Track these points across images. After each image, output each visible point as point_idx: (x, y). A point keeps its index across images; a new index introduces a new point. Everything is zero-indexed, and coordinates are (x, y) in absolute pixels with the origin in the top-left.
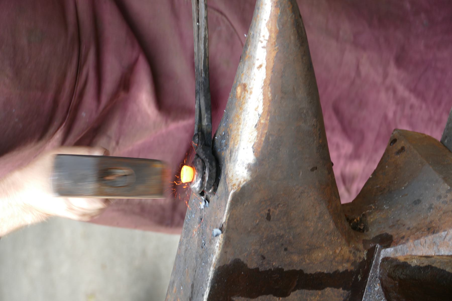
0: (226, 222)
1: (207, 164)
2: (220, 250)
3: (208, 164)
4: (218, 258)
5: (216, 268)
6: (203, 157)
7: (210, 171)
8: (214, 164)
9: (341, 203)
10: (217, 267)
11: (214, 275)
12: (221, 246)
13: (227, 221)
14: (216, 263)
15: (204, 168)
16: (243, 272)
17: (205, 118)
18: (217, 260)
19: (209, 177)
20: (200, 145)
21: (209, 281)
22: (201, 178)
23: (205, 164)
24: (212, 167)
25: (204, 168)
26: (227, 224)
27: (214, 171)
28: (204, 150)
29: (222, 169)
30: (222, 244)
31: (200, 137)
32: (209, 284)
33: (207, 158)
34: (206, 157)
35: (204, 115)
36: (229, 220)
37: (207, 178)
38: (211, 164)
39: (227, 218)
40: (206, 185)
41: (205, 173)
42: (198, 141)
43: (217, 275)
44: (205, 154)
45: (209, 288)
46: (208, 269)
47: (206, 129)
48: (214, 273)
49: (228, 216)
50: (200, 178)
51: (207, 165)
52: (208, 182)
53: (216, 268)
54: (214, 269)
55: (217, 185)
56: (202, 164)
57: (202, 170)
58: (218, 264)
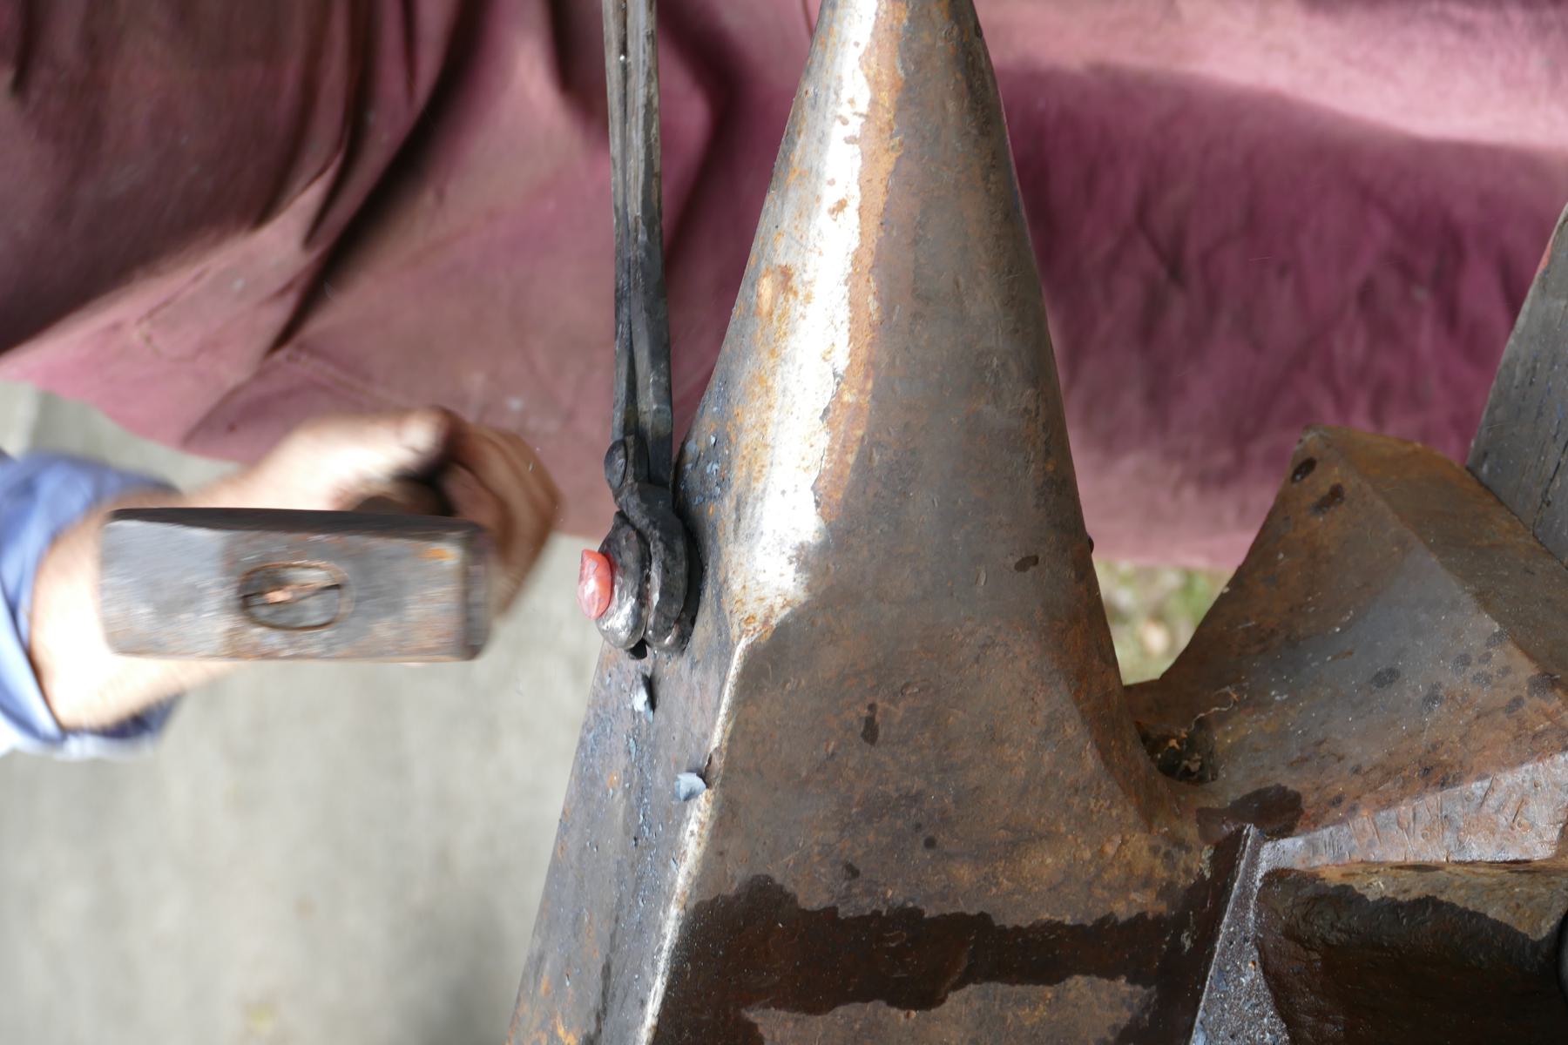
0: (723, 747)
1: (655, 546)
2: (703, 845)
3: (660, 546)
4: (695, 872)
8: (680, 546)
10: (692, 904)
11: (680, 931)
12: (705, 833)
13: (725, 744)
14: (688, 892)
15: (645, 561)
18: (690, 881)
20: (630, 480)
24: (674, 558)
25: (645, 561)
26: (725, 753)
28: (643, 498)
29: (707, 564)
30: (709, 825)
31: (631, 452)
33: (655, 528)
36: (731, 739)
37: (655, 597)
38: (669, 548)
39: (727, 736)
41: (648, 578)
42: (623, 467)
44: (649, 512)
45: (665, 979)
46: (661, 913)
48: (680, 927)
49: (730, 726)
51: (657, 549)
54: (682, 913)
56: (640, 548)
58: (695, 894)
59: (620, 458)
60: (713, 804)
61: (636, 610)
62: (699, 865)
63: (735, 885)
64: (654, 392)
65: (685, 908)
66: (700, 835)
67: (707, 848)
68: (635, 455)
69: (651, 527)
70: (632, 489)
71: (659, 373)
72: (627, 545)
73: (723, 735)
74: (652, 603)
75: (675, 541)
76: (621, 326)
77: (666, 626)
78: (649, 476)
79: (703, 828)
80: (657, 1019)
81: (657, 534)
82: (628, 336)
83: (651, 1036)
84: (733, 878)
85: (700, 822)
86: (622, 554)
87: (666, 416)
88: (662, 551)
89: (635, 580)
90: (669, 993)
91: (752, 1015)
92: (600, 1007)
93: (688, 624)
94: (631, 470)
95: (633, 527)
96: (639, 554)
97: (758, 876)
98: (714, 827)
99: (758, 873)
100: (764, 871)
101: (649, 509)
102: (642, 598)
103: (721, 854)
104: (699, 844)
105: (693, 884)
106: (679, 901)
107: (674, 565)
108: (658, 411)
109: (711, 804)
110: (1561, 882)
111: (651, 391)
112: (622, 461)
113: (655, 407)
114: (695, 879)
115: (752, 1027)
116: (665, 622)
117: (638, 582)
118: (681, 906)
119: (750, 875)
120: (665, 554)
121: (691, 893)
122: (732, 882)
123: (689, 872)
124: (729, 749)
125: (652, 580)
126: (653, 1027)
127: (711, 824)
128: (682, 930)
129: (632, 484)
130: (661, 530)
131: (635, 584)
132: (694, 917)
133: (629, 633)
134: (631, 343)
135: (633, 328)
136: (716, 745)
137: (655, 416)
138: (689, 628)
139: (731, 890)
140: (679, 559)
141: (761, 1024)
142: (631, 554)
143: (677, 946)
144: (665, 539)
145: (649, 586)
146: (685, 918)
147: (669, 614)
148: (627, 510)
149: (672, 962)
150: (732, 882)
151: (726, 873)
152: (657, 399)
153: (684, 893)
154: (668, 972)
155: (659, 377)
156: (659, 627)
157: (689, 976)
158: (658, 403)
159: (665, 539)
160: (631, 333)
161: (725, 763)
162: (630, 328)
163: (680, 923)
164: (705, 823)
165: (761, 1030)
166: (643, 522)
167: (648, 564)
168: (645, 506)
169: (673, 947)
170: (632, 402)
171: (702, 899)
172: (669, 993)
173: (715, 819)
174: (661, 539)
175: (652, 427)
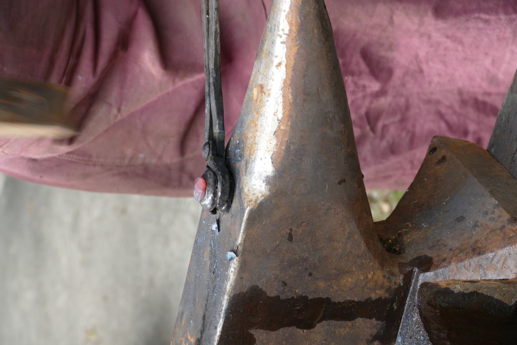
0: (242, 243)
1: (219, 177)
2: (235, 275)
3: (221, 177)
4: (233, 284)
5: (230, 297)
6: (215, 169)
8: (227, 177)
10: (232, 295)
11: (228, 304)
12: (236, 271)
13: (243, 242)
14: (231, 291)
15: (216, 182)
18: (231, 287)
20: (211, 155)
23: (217, 177)
25: (216, 182)
26: (242, 245)
30: (238, 269)
31: (211, 146)
33: (219, 171)
35: (216, 121)
36: (245, 240)
38: (224, 177)
39: (243, 239)
40: (218, 201)
41: (217, 188)
42: (208, 151)
44: (217, 166)
47: (218, 136)
48: (228, 303)
49: (244, 236)
51: (220, 178)
52: (220, 198)
54: (229, 298)
56: (214, 178)
57: (214, 184)
58: (233, 292)
59: (207, 148)
60: (239, 262)
64: (218, 126)
66: (235, 272)
67: (237, 276)
68: (212, 147)
69: (218, 171)
72: (210, 177)
73: (242, 239)
79: (235, 270)
80: (221, 333)
83: (219, 339)
84: (246, 286)
88: (221, 179)
89: (212, 188)
92: (202, 329)
93: (230, 202)
97: (254, 286)
98: (239, 269)
99: (254, 284)
100: (256, 284)
101: (217, 165)
102: (215, 194)
103: (241, 278)
104: (234, 275)
109: (238, 262)
111: (217, 126)
114: (233, 286)
115: (252, 335)
120: (222, 179)
121: (232, 291)
122: (245, 287)
124: (244, 244)
130: (221, 172)
136: (240, 242)
137: (219, 134)
141: (255, 334)
143: (227, 309)
145: (217, 190)
146: (230, 300)
148: (210, 165)
149: (225, 314)
154: (224, 317)
155: (220, 121)
157: (231, 318)
159: (222, 174)
160: (210, 107)
161: (243, 248)
162: (210, 105)
163: (228, 301)
164: (236, 268)
165: (255, 336)
166: (215, 169)
168: (215, 164)
169: (226, 309)
172: (225, 324)
173: (239, 267)
174: (221, 175)
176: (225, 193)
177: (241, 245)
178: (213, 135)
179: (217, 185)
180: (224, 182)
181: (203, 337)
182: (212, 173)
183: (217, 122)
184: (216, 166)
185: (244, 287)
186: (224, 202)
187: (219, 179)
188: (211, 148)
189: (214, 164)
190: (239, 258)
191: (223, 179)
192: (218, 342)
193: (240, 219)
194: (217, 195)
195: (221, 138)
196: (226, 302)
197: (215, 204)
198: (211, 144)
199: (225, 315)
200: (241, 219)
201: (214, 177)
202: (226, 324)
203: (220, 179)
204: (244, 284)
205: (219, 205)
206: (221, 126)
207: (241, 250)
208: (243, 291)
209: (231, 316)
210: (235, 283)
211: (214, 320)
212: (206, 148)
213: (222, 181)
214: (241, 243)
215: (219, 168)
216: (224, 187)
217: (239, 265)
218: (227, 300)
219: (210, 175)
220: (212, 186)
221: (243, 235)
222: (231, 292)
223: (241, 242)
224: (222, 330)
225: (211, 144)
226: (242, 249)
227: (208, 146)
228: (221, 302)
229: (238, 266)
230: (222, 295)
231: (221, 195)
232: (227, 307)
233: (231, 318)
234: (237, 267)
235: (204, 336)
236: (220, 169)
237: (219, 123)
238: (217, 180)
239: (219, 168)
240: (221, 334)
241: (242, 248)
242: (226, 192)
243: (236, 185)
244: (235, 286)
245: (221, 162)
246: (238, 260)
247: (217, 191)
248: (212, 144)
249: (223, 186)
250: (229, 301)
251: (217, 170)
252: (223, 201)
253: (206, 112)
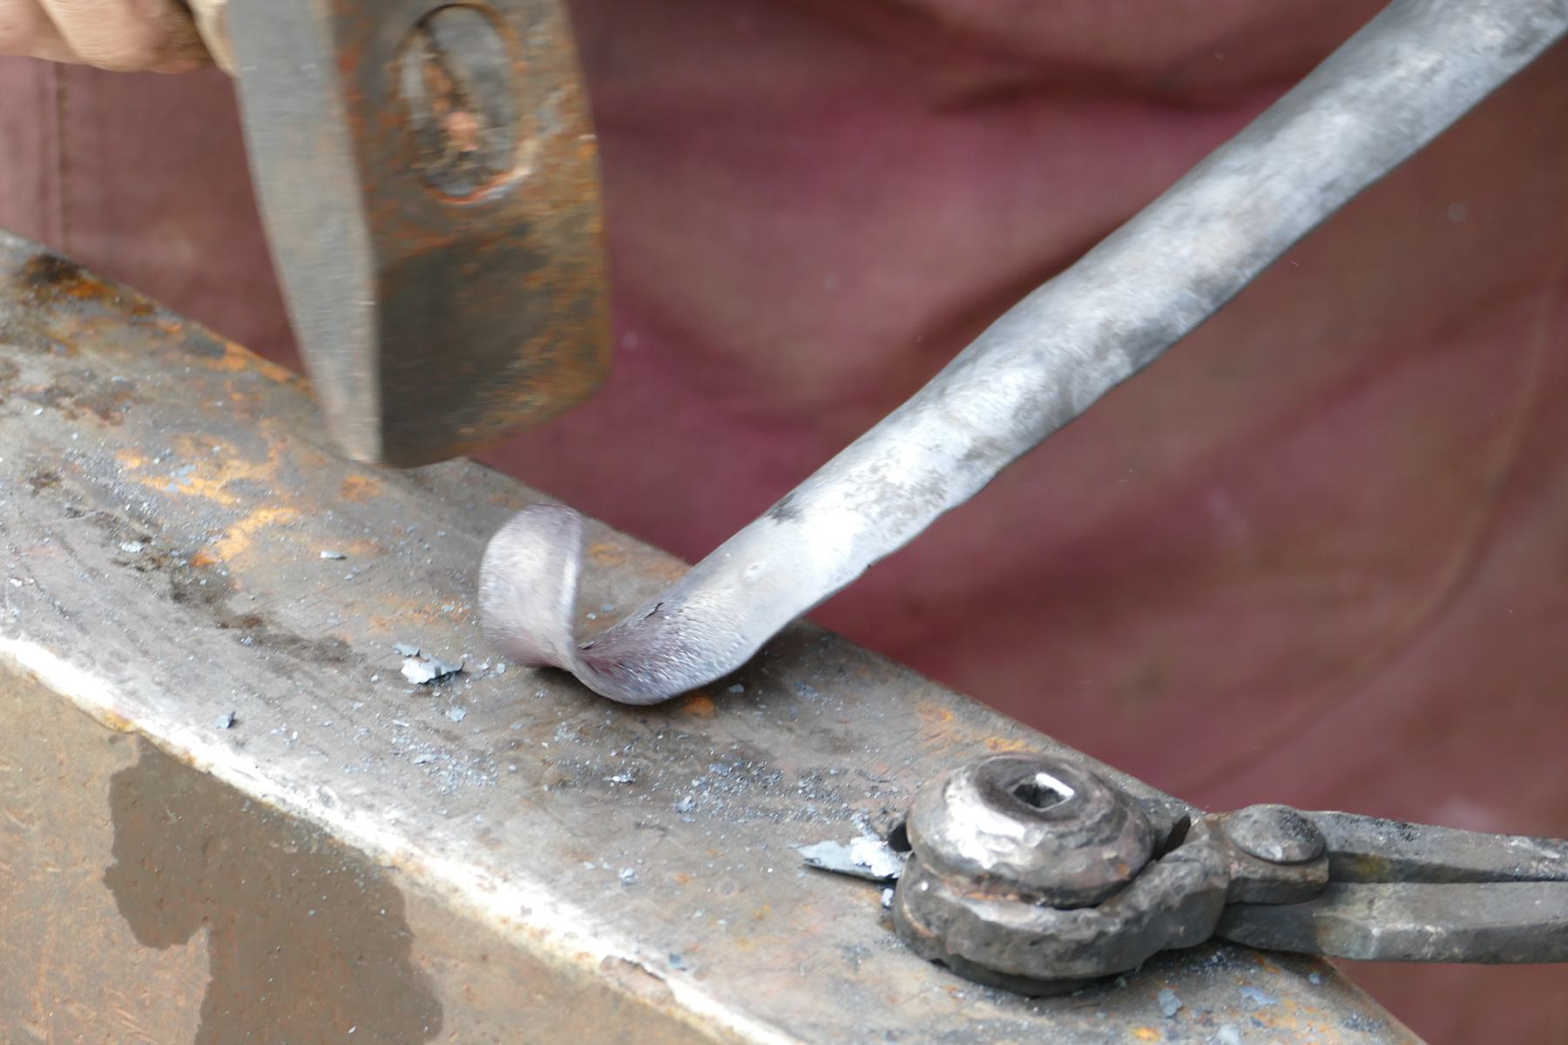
0: (673, 1008)
1: (1089, 922)
2: (502, 929)
3: (1087, 934)
4: (455, 901)
5: (390, 872)
6: (1143, 897)
7: (1037, 940)
8: (1083, 968)
9: (894, 894)
10: (399, 881)
11: (353, 849)
12: (522, 938)
13: (678, 1015)
14: (422, 881)
15: (1064, 898)
16: (315, 915)
17: (1419, 916)
18: (441, 889)
19: (993, 927)
20: (1236, 869)
21: (316, 811)
22: (994, 866)
23: (1093, 906)
24: (1059, 957)
25: (1064, 898)
26: (663, 1009)
27: (1034, 966)
28: (1191, 900)
29: (1041, 1013)
30: (537, 949)
31: (1293, 874)
32: (303, 803)
33: (1127, 922)
34: (1138, 917)
35: (1441, 915)
36: (685, 1029)
37: (988, 912)
38: (1083, 949)
39: (693, 1021)
40: (947, 894)
41: (1027, 898)
42: (1264, 855)
43: (351, 873)
44: (1162, 910)
45: (271, 800)
46: (396, 814)
47: (1345, 922)
48: (361, 852)
49: (709, 1031)
50: (995, 860)
51: (1086, 923)
52: (964, 912)
53: (390, 872)
54: (386, 861)
55: (944, 959)
56: (1091, 889)
57: (1047, 884)
58: (417, 892)
59: (1284, 850)
60: (574, 967)
61: (969, 867)
62: (467, 913)
63: (429, 970)
64: (1406, 932)
65: (393, 867)
66: (519, 927)
67: (496, 934)
68: (1286, 882)
69: (1129, 914)
70: (1216, 874)
71: (1445, 943)
72: (1102, 862)
73: (695, 1015)
74: (977, 901)
75: (1095, 960)
76: (1556, 856)
77: (933, 918)
78: (1241, 903)
79: (533, 935)
80: (203, 770)
81: (1113, 929)
82: (1532, 872)
83: (175, 752)
84: (441, 968)
85: (543, 933)
86: (1086, 849)
87: (1354, 951)
88: (1076, 936)
89: (1027, 873)
90: (248, 804)
91: (200, 938)
92: (271, 630)
93: (935, 955)
94: (1259, 871)
95: (1142, 871)
96: (1077, 886)
97: (440, 1013)
98: (532, 957)
99: (447, 1015)
100: (448, 1027)
101: (1169, 909)
102: (992, 882)
103: (484, 958)
104: (505, 921)
105: (435, 892)
106: (407, 860)
107: (1045, 956)
108: (1367, 936)
109: (574, 961)
110: (1257, 836)
111: (1410, 926)
112: (1278, 854)
113: (1376, 931)
114: (444, 899)
115: (182, 938)
116: (939, 917)
117: (1022, 878)
118: (399, 861)
119: (442, 1000)
120: (1071, 941)
121: (419, 885)
122: (434, 965)
123: (456, 890)
124: (667, 1019)
125: (1023, 906)
126: (190, 761)
127: (538, 953)
128: (354, 854)
129: (1226, 873)
130: (1120, 936)
131: (1018, 873)
132: (376, 882)
133: (930, 844)
134: (1518, 879)
135: (1547, 884)
136: (679, 997)
137: (1358, 928)
138: (926, 953)
139: (420, 956)
140: (1058, 966)
141: (185, 951)
142: (1079, 870)
143: (330, 837)
144: (1102, 942)
145: (1011, 897)
146: (377, 866)
147: (953, 929)
148: (1178, 859)
149: (303, 821)
150: (434, 965)
151: (449, 957)
152: (1389, 938)
153: (421, 870)
154: (284, 809)
155: (1434, 944)
156: (932, 906)
157: (275, 846)
158: (1382, 939)
159: (1102, 942)
160: (1538, 879)
161: (645, 1006)
162: (1548, 879)
163: (368, 852)
164: (540, 941)
165: (175, 949)
166: (1143, 897)
167: (1057, 901)
168: (1176, 901)
169: (328, 830)
170: (1401, 871)
171: (407, 902)
172: (248, 804)
173: (547, 962)
174: (1101, 934)
175: (1336, 919)
176: (988, 944)
177: (661, 1002)
178: (1362, 880)
179: (1044, 905)
180: (1056, 952)
181: (221, 631)
182: (1125, 873)
183: (1430, 928)
184: (1159, 905)
185: (437, 960)
186: (938, 927)
187: (1075, 920)
188: (1283, 873)
189: (1181, 888)
190: (592, 972)
191: (1073, 946)
192: (156, 742)
193: (812, 1019)
194: (988, 892)
195: (1332, 937)
196: (363, 840)
197: (934, 866)
198: (1304, 876)
199: (294, 819)
200: (814, 1026)
201: (1097, 888)
202: (250, 808)
203: (1078, 929)
204: (453, 962)
205: (928, 895)
206: (1401, 946)
207: (634, 993)
208: (415, 946)
209: (286, 850)
210: (463, 919)
211: (288, 733)
212: (1287, 844)
213: (1064, 937)
214: (673, 1002)
215: (1146, 920)
216: (1026, 947)
217: (557, 963)
218: (375, 850)
219: (1114, 862)
220: (1043, 868)
221: (718, 1029)
222: (415, 884)
223: (679, 1006)
224: (216, 778)
225: (1304, 876)
226: (641, 1000)
227: (1296, 855)
228: (377, 802)
229: (552, 957)
230: (413, 821)
231: (977, 918)
232: (337, 836)
233: (275, 846)
234: (547, 947)
235: (223, 642)
236: (1135, 930)
237: (1423, 936)
238: (1072, 901)
239: (1146, 920)
240: (200, 773)
241: (648, 1001)
242: (994, 949)
243: (1030, 1008)
244: (446, 910)
245: (1182, 929)
246: (585, 965)
247: (1005, 895)
248: (1305, 882)
249: (1033, 944)
250: (367, 858)
251: (1135, 909)
252: (947, 923)
253: (1516, 842)
